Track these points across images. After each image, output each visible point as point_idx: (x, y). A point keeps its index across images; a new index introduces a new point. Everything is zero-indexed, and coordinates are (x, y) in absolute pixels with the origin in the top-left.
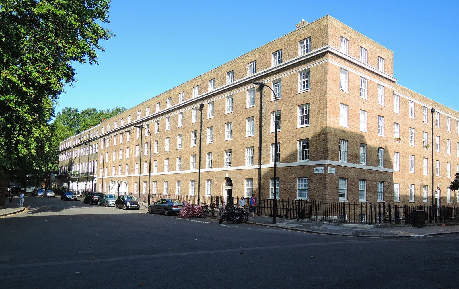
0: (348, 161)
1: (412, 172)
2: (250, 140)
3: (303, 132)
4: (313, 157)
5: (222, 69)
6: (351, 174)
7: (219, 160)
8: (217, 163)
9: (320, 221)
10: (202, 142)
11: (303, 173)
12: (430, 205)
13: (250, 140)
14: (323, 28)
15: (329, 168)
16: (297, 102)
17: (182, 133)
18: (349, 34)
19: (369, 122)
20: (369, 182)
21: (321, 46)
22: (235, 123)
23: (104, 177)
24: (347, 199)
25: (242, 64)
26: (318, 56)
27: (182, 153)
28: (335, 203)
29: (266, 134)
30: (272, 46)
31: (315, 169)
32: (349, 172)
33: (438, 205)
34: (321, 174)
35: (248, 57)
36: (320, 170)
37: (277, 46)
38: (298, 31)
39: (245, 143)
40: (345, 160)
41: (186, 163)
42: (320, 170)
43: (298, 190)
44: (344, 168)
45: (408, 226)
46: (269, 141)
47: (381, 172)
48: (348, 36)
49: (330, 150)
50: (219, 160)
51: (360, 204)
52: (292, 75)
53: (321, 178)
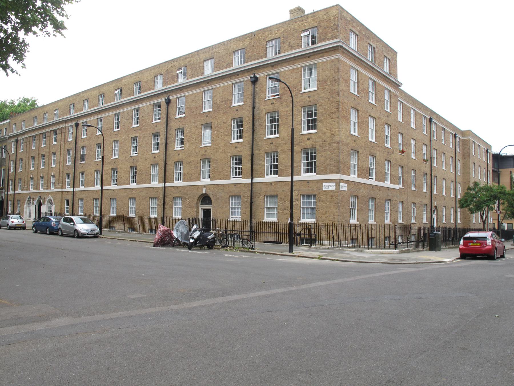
0: (359, 176)
1: (413, 188)
2: (236, 147)
3: (308, 139)
4: (322, 171)
5: (197, 56)
6: (361, 191)
7: (193, 171)
8: (190, 176)
9: (338, 247)
10: (168, 148)
11: (309, 190)
12: (428, 226)
13: (236, 147)
14: (332, 18)
15: (341, 184)
16: (301, 103)
17: (137, 135)
18: (358, 28)
19: (377, 130)
20: (378, 201)
21: (330, 39)
22: (216, 125)
23: (16, 192)
24: (358, 221)
25: (226, 51)
26: (327, 50)
27: (138, 161)
28: (364, 226)
29: (258, 140)
30: (267, 33)
31: (324, 184)
32: (360, 189)
33: (435, 226)
34: (331, 191)
35: (234, 43)
36: (331, 187)
37: (274, 34)
38: (301, 19)
39: (229, 150)
40: (355, 174)
41: (144, 175)
42: (330, 186)
43: (265, 209)
44: (355, 184)
45: (426, 250)
46: (263, 149)
47: (388, 189)
48: (357, 30)
49: (342, 163)
50: (193, 171)
51: (386, 226)
52: (294, 69)
53: (332, 196)
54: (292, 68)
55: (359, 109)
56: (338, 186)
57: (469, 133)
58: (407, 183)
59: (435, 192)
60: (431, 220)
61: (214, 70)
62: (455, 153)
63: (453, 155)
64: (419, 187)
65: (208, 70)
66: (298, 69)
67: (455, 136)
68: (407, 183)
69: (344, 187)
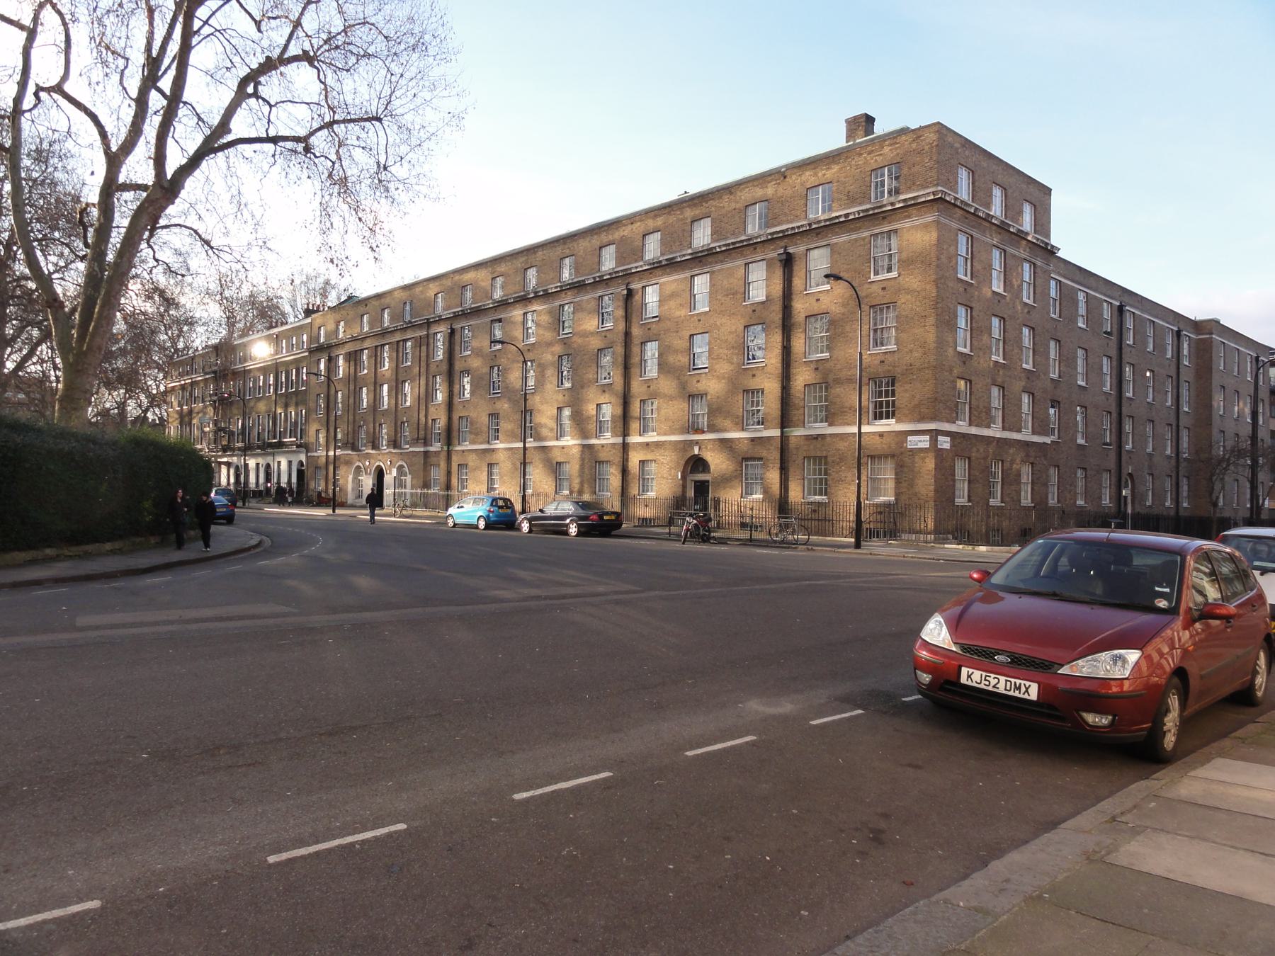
15: (940, 438)
31: (910, 438)
33: (1129, 511)
36: (923, 442)
52: (856, 240)
54: (853, 237)
55: (973, 305)
56: (934, 441)
57: (1212, 326)
58: (1066, 426)
59: (1129, 447)
60: (1118, 498)
61: (713, 240)
62: (1178, 368)
63: (1173, 373)
64: (1160, 347)
65: (702, 236)
66: (863, 239)
67: (1178, 333)
68: (1066, 426)
69: (944, 443)
